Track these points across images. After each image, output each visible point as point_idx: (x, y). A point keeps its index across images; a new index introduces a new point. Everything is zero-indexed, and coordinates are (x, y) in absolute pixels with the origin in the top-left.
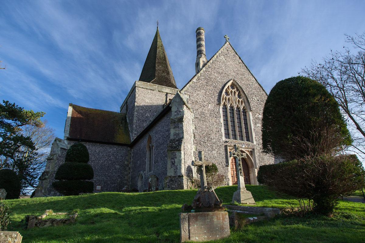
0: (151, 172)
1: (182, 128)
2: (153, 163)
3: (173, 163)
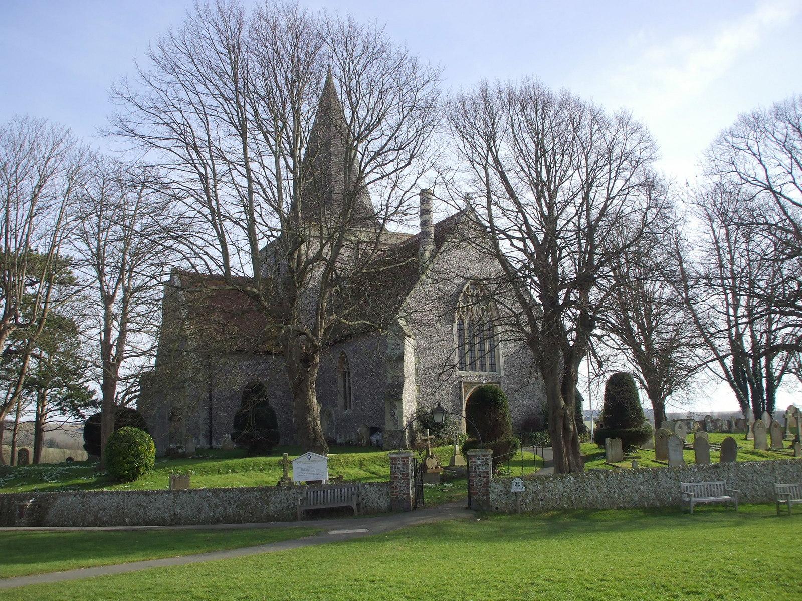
0: (346, 412)
1: (402, 368)
2: (353, 398)
3: (393, 415)
